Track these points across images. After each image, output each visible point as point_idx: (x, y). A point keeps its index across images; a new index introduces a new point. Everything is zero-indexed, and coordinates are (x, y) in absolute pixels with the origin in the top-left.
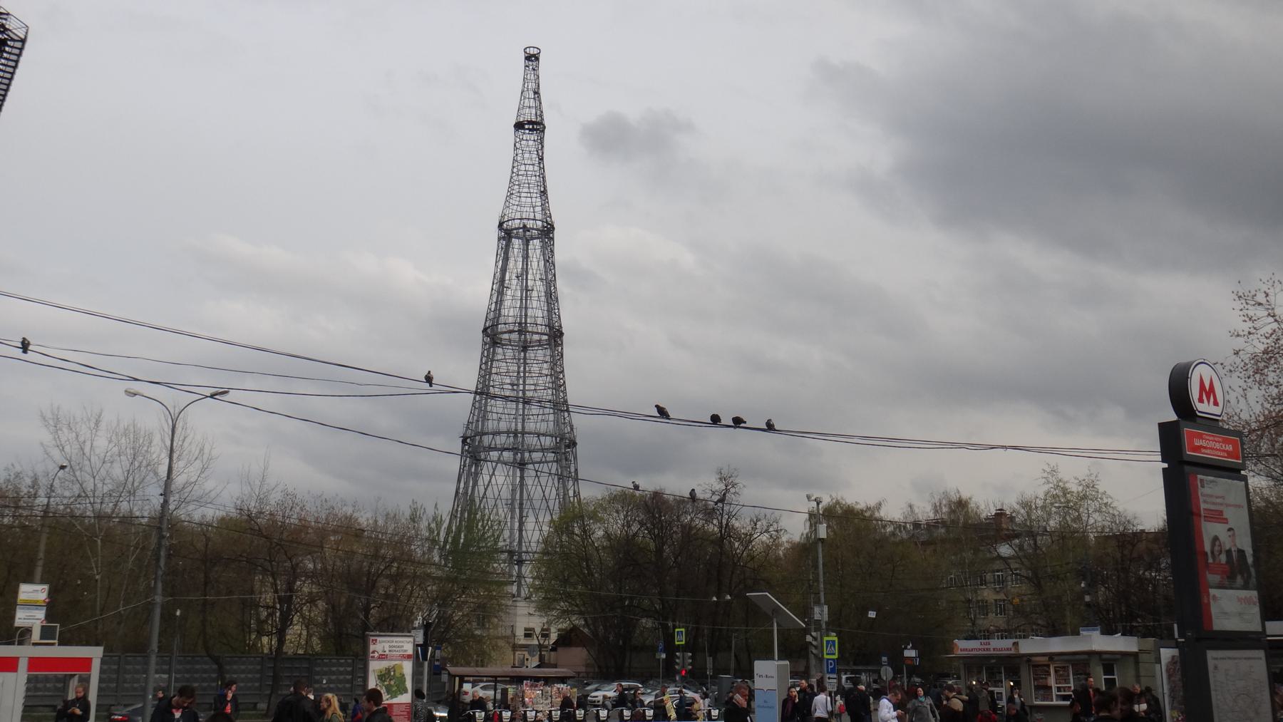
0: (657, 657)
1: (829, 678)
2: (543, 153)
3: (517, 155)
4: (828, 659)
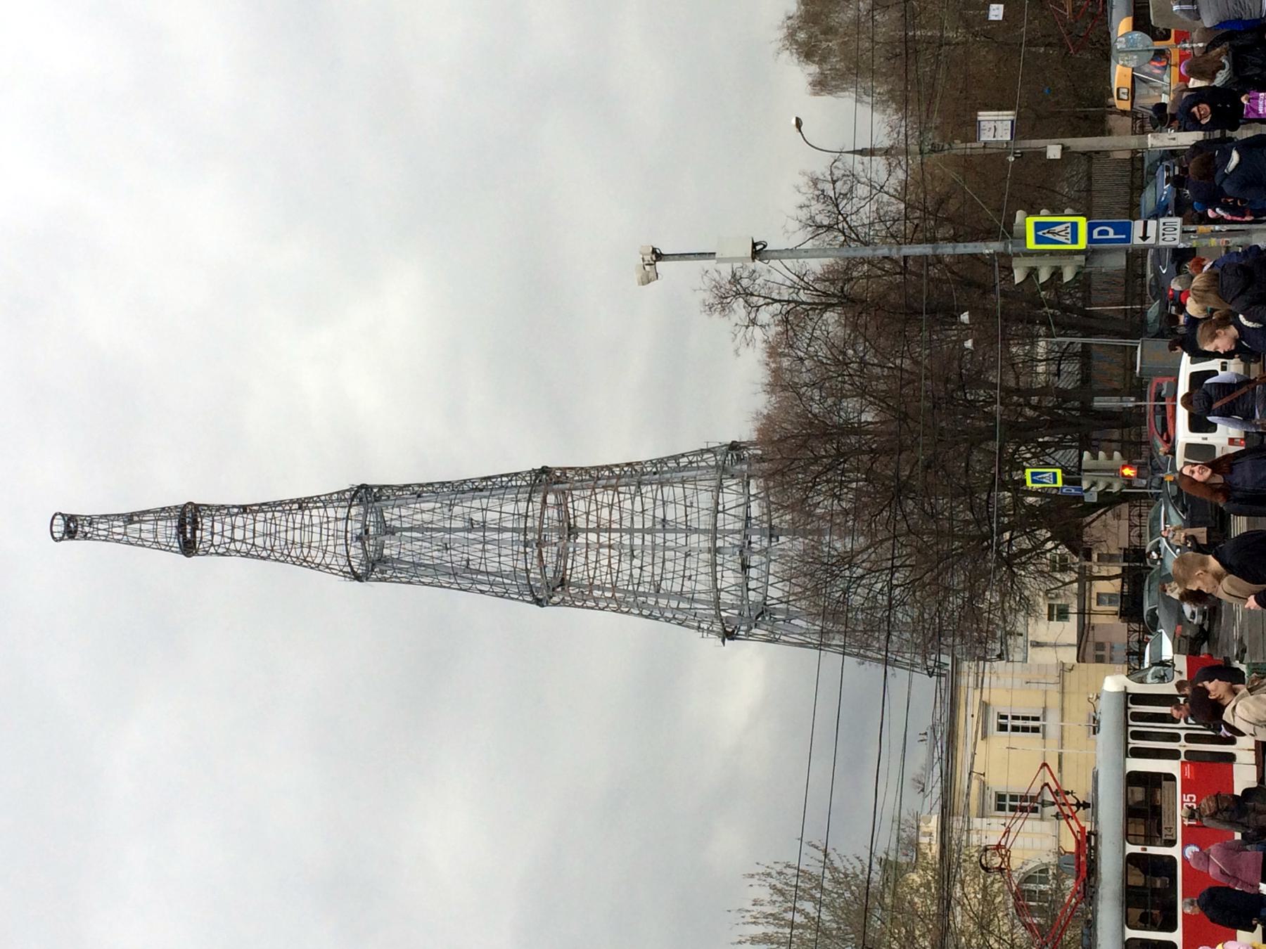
1: (1145, 237)
2: (234, 506)
3: (239, 552)
4: (1090, 239)
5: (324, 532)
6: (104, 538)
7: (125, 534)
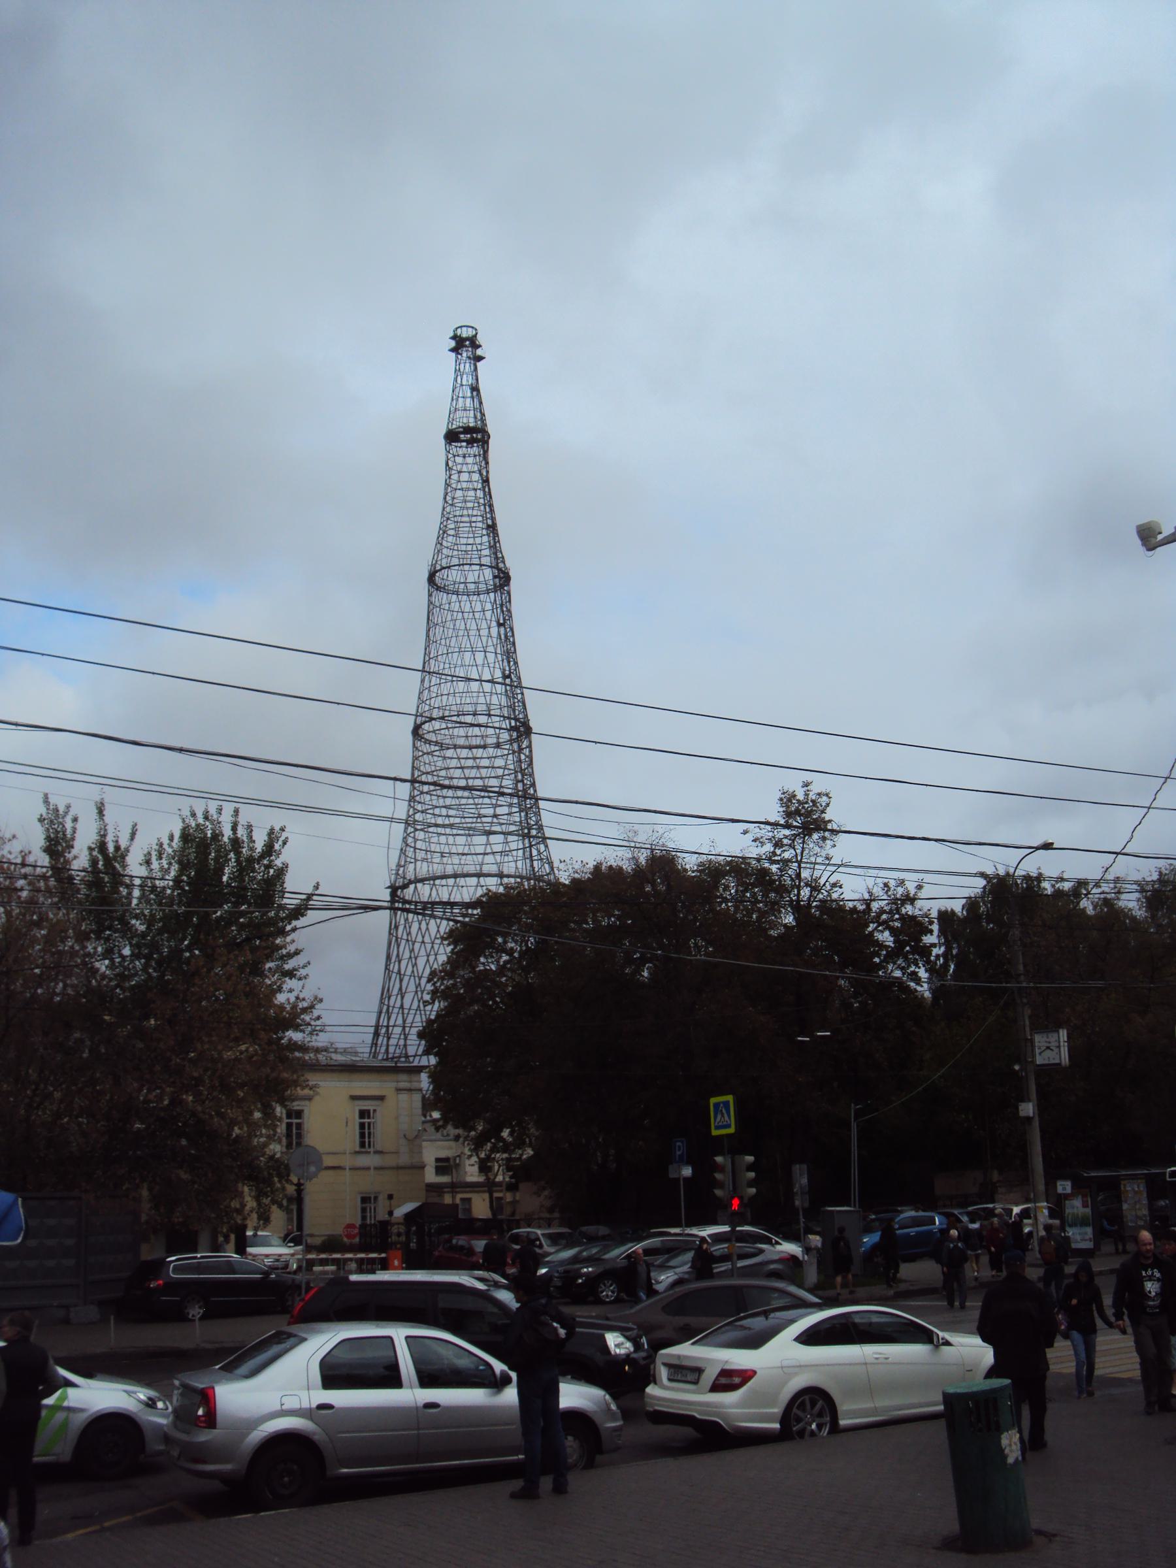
0: (672, 1175)
2: (488, 472)
5: (469, 547)
6: (457, 368)
7: (462, 385)
